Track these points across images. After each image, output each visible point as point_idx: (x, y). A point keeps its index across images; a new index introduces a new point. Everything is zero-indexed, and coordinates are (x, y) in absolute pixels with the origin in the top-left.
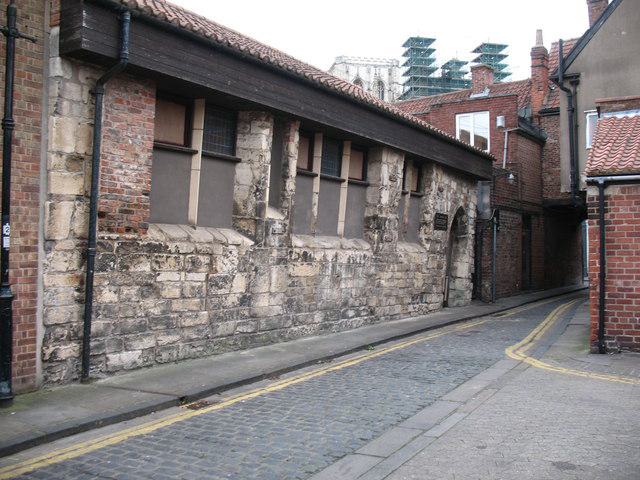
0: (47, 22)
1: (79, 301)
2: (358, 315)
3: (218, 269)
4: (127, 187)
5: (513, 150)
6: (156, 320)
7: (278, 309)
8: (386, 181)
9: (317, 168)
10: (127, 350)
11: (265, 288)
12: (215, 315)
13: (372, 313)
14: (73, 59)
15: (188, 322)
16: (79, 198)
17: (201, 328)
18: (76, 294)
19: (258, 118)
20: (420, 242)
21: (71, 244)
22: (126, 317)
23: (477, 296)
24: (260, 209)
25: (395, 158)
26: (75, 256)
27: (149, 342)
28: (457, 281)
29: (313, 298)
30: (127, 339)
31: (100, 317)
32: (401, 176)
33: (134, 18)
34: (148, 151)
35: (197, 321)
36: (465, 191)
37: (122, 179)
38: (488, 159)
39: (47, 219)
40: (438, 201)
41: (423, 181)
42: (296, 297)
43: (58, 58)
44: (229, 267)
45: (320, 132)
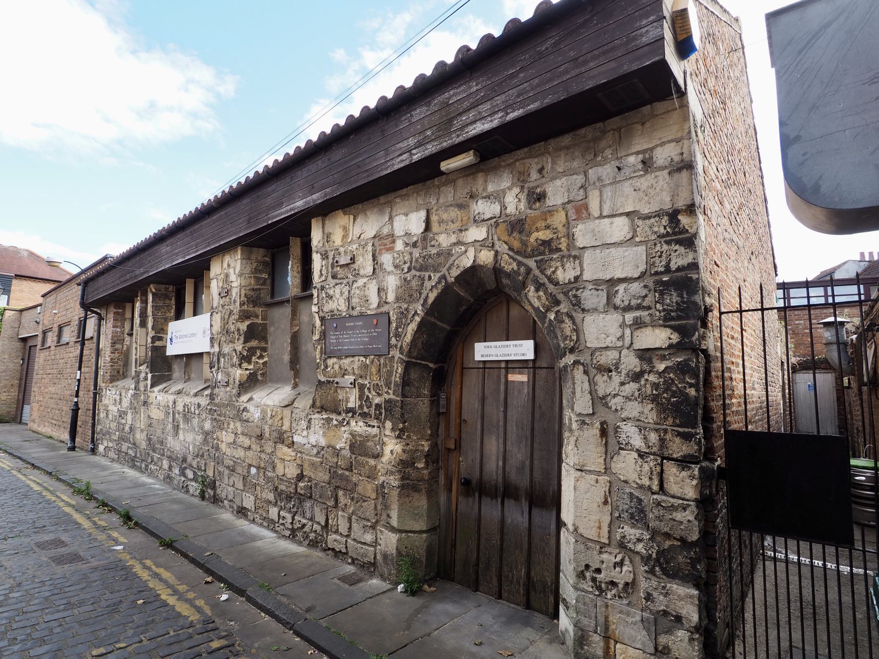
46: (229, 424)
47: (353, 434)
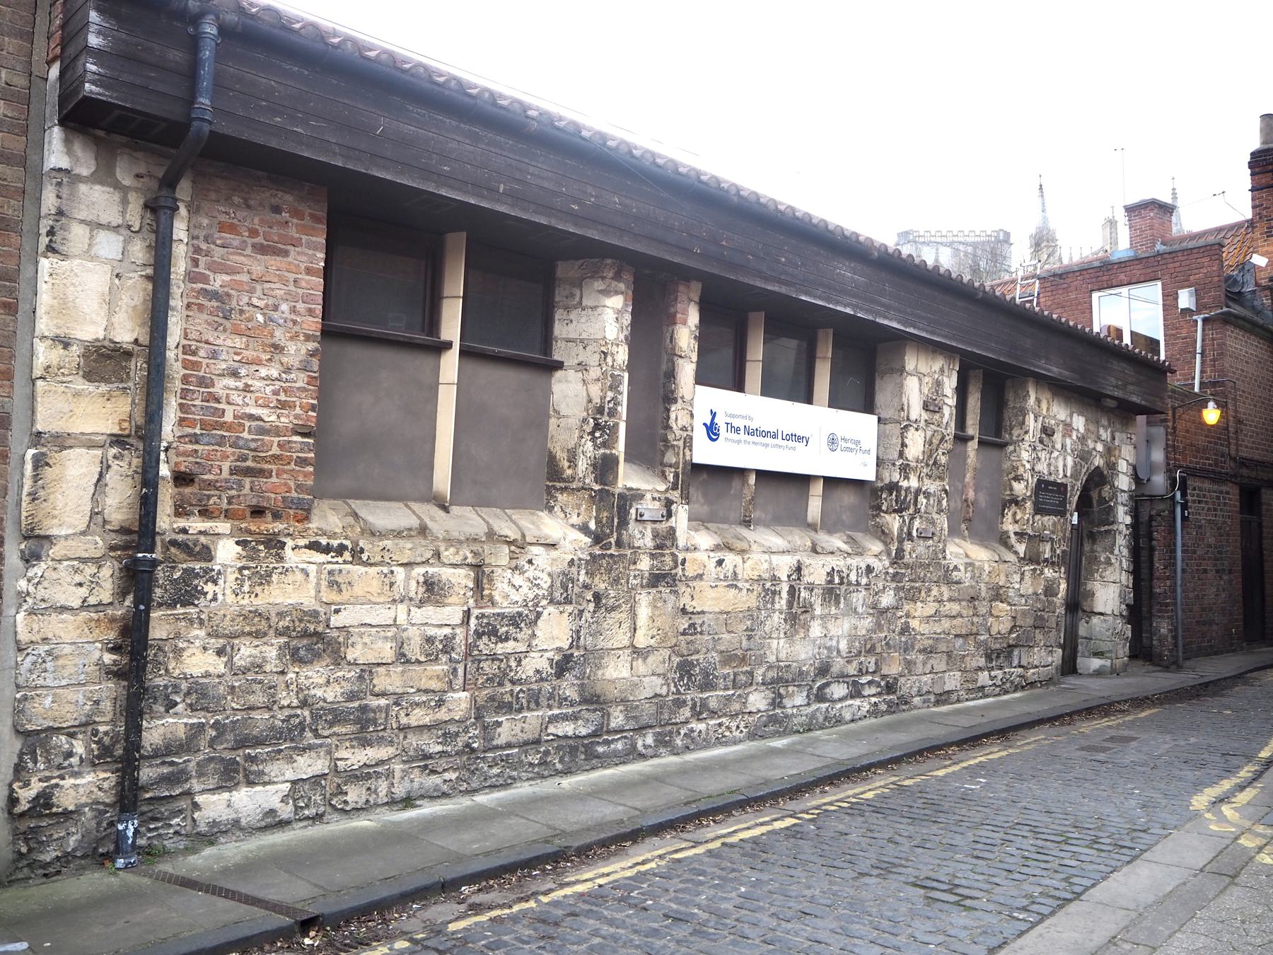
0: (40, 54)
1: (116, 673)
2: (856, 692)
3: (497, 598)
4: (251, 417)
5: (1214, 357)
6: (337, 717)
7: (654, 685)
8: (916, 411)
9: (972, 429)
10: (251, 783)
11: (621, 638)
12: (492, 699)
13: (890, 688)
14: (101, 133)
15: (419, 717)
16: (118, 440)
17: (453, 729)
18: (108, 658)
19: (596, 274)
20: (1004, 540)
21: (96, 544)
22: (251, 708)
23: (1141, 651)
24: (605, 468)
25: (938, 364)
26: (106, 572)
27: (309, 765)
28: (1095, 620)
29: (743, 660)
30: (251, 759)
31: (180, 708)
32: (951, 401)
33: (224, 31)
34: (308, 338)
35: (442, 715)
36: (1105, 434)
37: (236, 398)
38: (1160, 371)
39: (26, 489)
40: (1043, 455)
41: (1008, 414)
42: (701, 657)
43: (56, 129)
44: (526, 592)
45: (757, 309)
46: (930, 590)
47: (1046, 580)
